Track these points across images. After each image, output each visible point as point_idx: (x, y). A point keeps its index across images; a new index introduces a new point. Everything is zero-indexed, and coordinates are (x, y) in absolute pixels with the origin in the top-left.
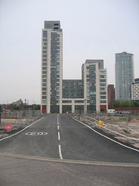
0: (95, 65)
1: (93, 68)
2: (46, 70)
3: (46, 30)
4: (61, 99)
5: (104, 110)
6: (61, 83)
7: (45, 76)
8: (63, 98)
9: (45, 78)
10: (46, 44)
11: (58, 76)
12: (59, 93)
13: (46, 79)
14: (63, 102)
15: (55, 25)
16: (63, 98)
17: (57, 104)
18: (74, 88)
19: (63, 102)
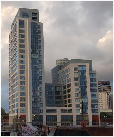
0: (85, 66)
1: (62, 65)
2: (92, 88)
3: (22, 19)
4: (45, 108)
5: (96, 121)
6: (44, 86)
7: (23, 78)
8: (46, 106)
9: (23, 80)
10: (23, 36)
11: (41, 78)
12: (41, 99)
13: (24, 80)
14: (48, 111)
15: (33, 14)
16: (46, 106)
17: (41, 114)
18: (51, 89)
19: (48, 111)
